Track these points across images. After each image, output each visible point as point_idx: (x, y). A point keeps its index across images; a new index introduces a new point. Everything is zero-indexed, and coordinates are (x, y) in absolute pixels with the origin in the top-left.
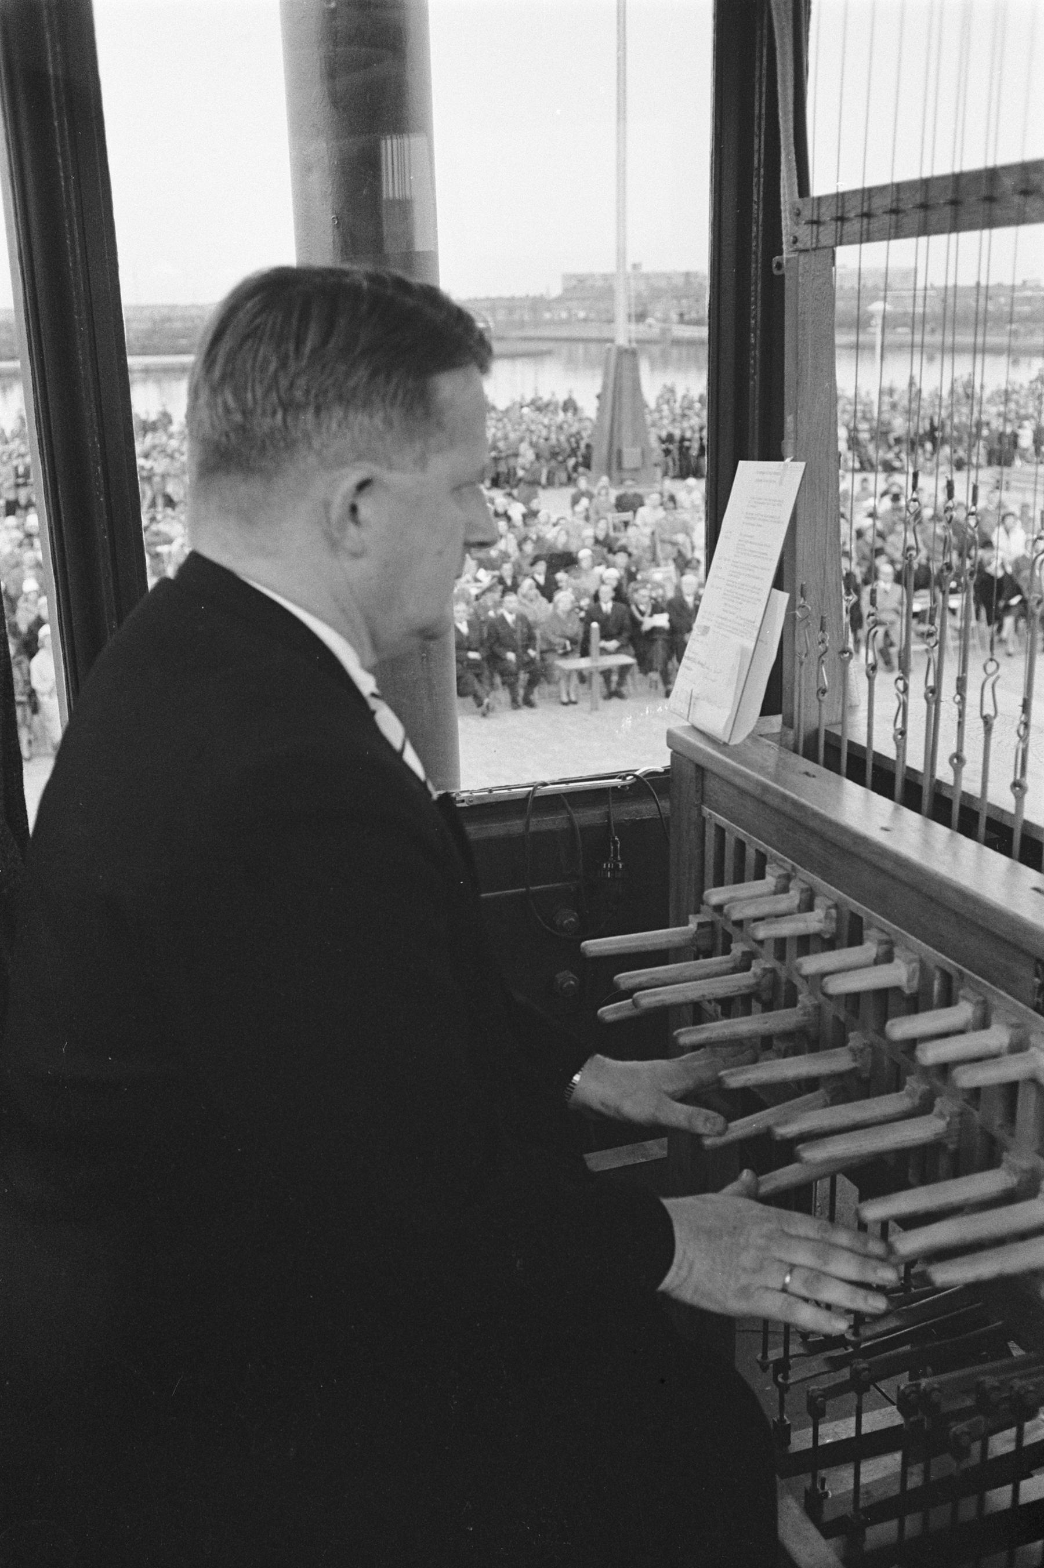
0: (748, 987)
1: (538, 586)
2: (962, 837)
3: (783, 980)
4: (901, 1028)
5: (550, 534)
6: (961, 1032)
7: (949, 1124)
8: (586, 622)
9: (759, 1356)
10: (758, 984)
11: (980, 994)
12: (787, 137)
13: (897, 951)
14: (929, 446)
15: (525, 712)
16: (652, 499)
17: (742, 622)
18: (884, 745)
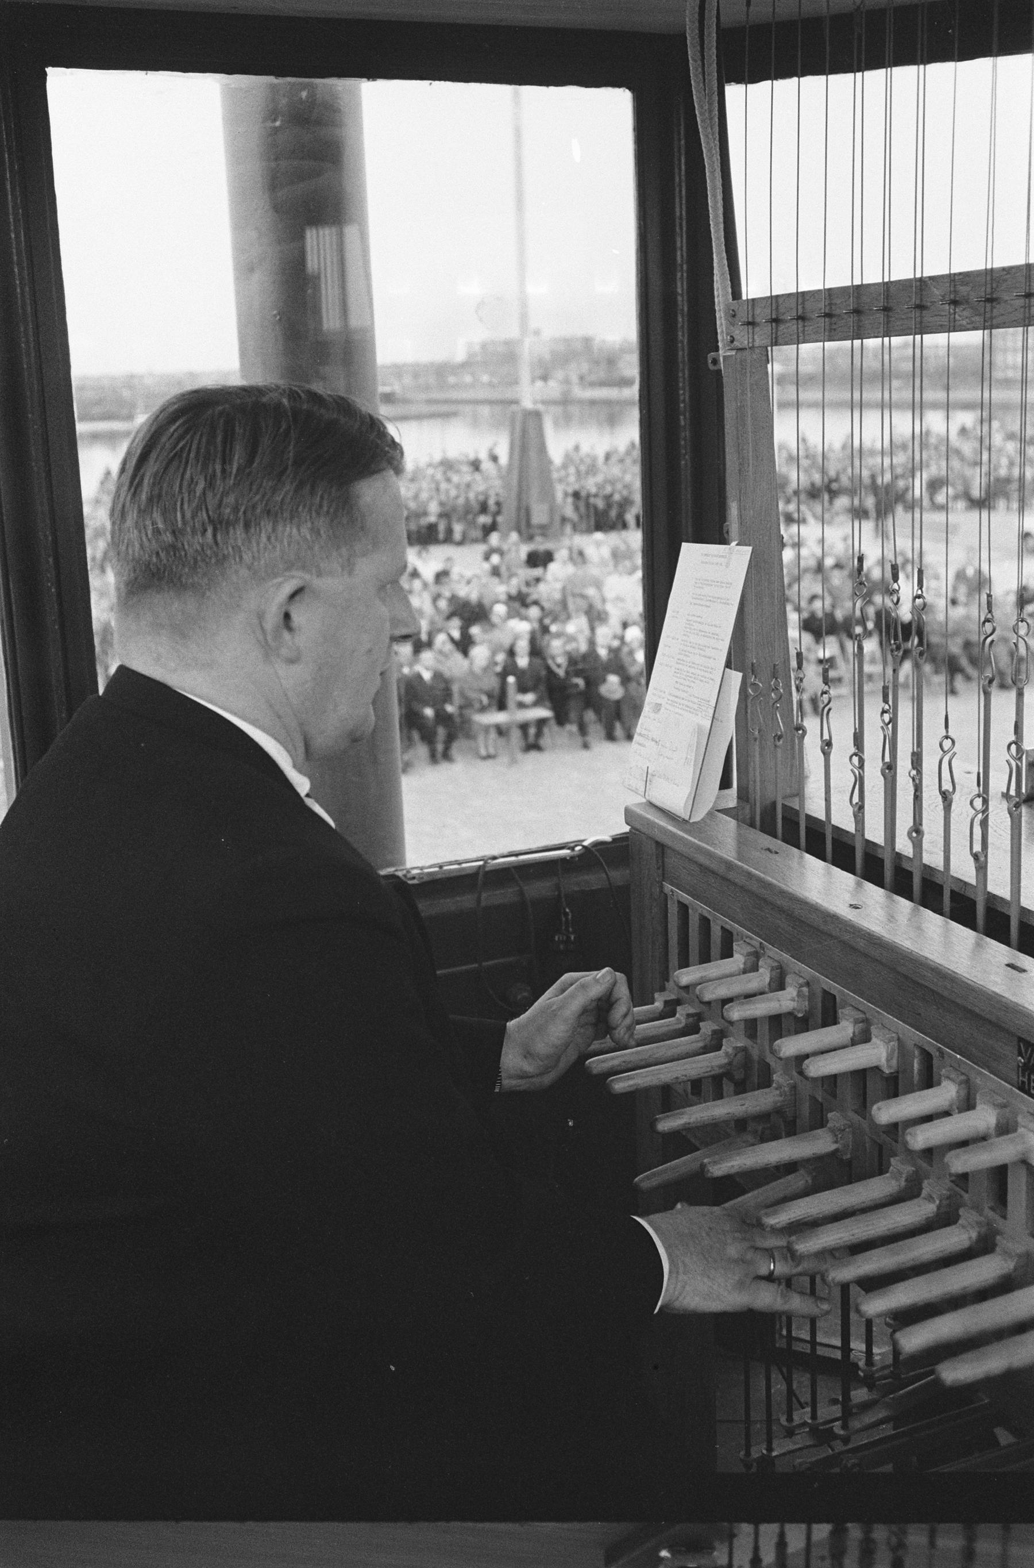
0: (720, 1067)
1: (452, 639)
2: (922, 908)
3: (756, 1058)
4: (887, 1112)
5: (463, 592)
6: (947, 1114)
7: (939, 1207)
8: (503, 676)
9: (742, 1453)
10: (730, 1064)
11: (963, 1074)
12: (718, 246)
13: (874, 1030)
14: (826, 497)
15: (444, 768)
16: (562, 554)
17: (696, 700)
18: (843, 819)
